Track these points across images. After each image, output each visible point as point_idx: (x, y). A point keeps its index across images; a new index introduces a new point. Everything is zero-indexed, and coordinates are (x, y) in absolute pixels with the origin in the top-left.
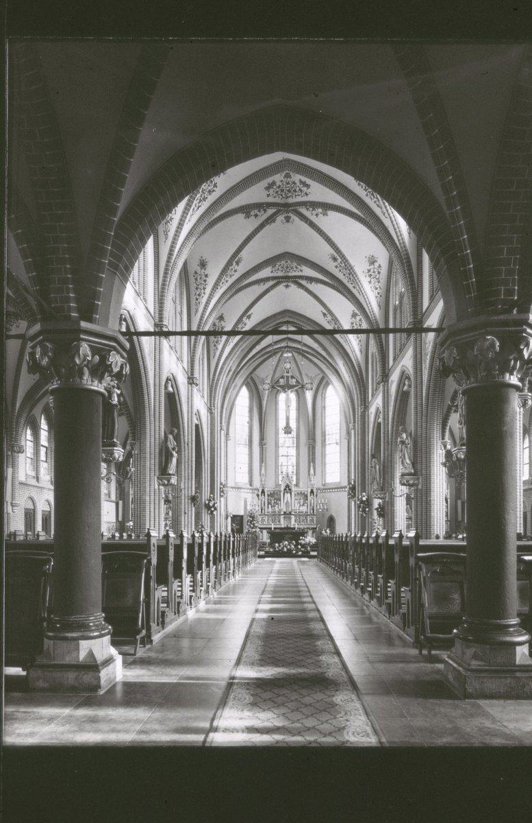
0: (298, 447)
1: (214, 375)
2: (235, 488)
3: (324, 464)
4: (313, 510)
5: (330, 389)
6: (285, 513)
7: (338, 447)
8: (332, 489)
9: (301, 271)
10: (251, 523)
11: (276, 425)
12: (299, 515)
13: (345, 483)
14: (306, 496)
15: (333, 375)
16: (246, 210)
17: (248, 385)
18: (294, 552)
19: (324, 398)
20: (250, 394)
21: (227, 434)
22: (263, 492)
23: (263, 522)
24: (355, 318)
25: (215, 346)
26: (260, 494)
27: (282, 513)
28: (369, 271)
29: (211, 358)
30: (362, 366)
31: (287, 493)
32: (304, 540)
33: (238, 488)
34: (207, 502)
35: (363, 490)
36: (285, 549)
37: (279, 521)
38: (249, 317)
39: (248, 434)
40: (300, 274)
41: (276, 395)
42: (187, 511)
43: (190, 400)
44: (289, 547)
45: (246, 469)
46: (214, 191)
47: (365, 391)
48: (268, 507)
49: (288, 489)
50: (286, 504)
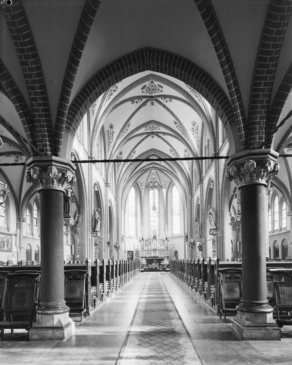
0: (159, 217)
1: (118, 182)
3: (172, 225)
5: (175, 189)
9: (160, 129)
12: (161, 250)
14: (164, 241)
16: (132, 99)
17: (134, 186)
18: (158, 269)
19: (172, 192)
22: (143, 239)
25: (118, 167)
27: (152, 249)
34: (115, 245)
36: (154, 268)
37: (151, 254)
38: (134, 153)
43: (106, 194)
44: (156, 266)
45: (134, 228)
46: (116, 90)
49: (155, 237)
50: (154, 245)
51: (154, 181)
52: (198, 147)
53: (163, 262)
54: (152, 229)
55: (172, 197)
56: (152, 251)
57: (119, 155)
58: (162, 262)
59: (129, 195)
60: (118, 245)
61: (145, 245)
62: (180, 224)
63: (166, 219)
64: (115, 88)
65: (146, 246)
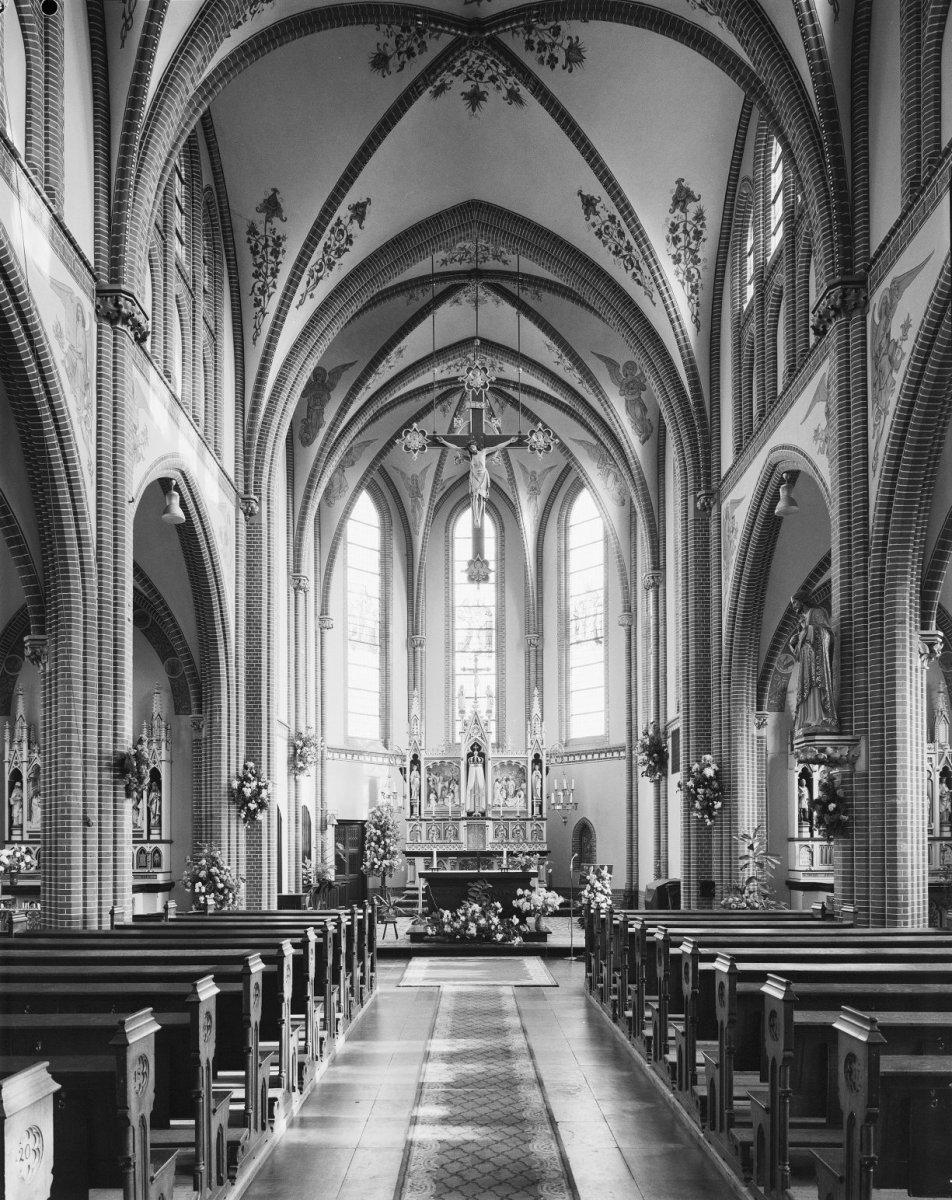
0: (500, 652)
1: (257, 395)
2: (346, 752)
3: (565, 693)
4: (541, 807)
5: (584, 499)
6: (470, 814)
7: (600, 650)
8: (586, 753)
10: (378, 842)
11: (447, 598)
12: (504, 819)
13: (622, 739)
14: (522, 771)
15: (590, 462)
17: (369, 489)
18: (499, 937)
19: (564, 529)
20: (382, 517)
21: (324, 611)
22: (415, 761)
23: (405, 836)
24: (684, 210)
26: (407, 765)
27: (464, 815)
28: (674, 228)
29: (249, 332)
30: (648, 480)
31: (476, 762)
32: (528, 900)
33: (353, 753)
34: (235, 784)
35: (704, 746)
36: (473, 930)
37: (456, 835)
38: (359, 211)
39: (377, 618)
40: (500, 266)
41: (448, 521)
42: (94, 815)
43: (108, 383)
44: (482, 921)
45: (374, 706)
46: (347, 250)
47: (708, 446)
48: (428, 800)
49: (477, 752)
50: (473, 791)
51: (478, 405)
52: (698, 327)
53: (527, 892)
54: (462, 712)
55: (564, 554)
56: (465, 823)
57: (263, 216)
58: (520, 892)
59: (351, 527)
60: (254, 784)
61: (429, 792)
62: (607, 687)
63: (533, 665)
64: (343, 241)
65: (432, 796)
